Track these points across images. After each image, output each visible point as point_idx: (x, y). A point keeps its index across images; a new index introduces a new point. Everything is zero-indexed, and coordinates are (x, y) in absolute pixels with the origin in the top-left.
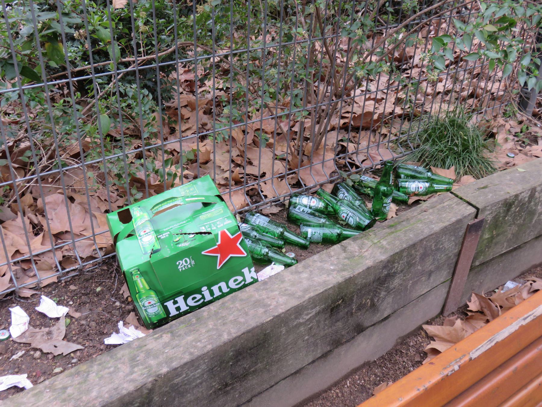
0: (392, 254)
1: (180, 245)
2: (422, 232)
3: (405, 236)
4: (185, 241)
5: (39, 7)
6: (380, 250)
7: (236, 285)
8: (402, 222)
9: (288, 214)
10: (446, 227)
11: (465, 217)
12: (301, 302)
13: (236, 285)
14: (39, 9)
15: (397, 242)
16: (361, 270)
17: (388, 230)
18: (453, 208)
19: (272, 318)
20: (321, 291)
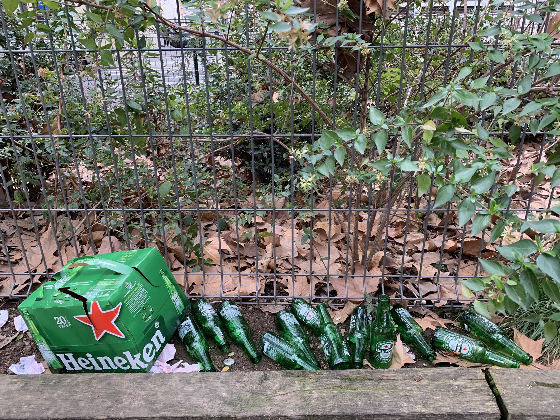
0: (307, 414)
1: (56, 302)
2: (380, 405)
3: (351, 400)
4: (61, 299)
5: (286, 290)
6: (299, 402)
7: (150, 356)
8: (369, 380)
9: (177, 330)
10: (424, 415)
11: (471, 415)
12: (150, 416)
13: (150, 356)
14: (287, 288)
15: (332, 402)
16: (249, 415)
17: (338, 382)
18: (463, 393)
19: (106, 417)
20: (183, 415)
